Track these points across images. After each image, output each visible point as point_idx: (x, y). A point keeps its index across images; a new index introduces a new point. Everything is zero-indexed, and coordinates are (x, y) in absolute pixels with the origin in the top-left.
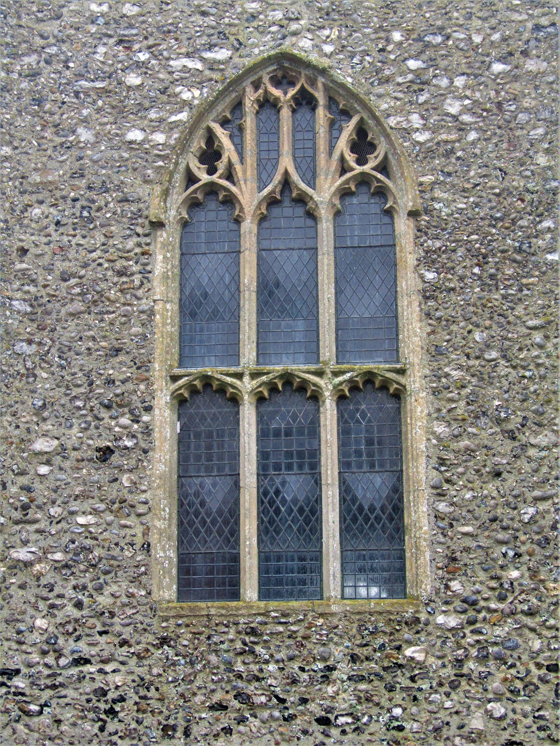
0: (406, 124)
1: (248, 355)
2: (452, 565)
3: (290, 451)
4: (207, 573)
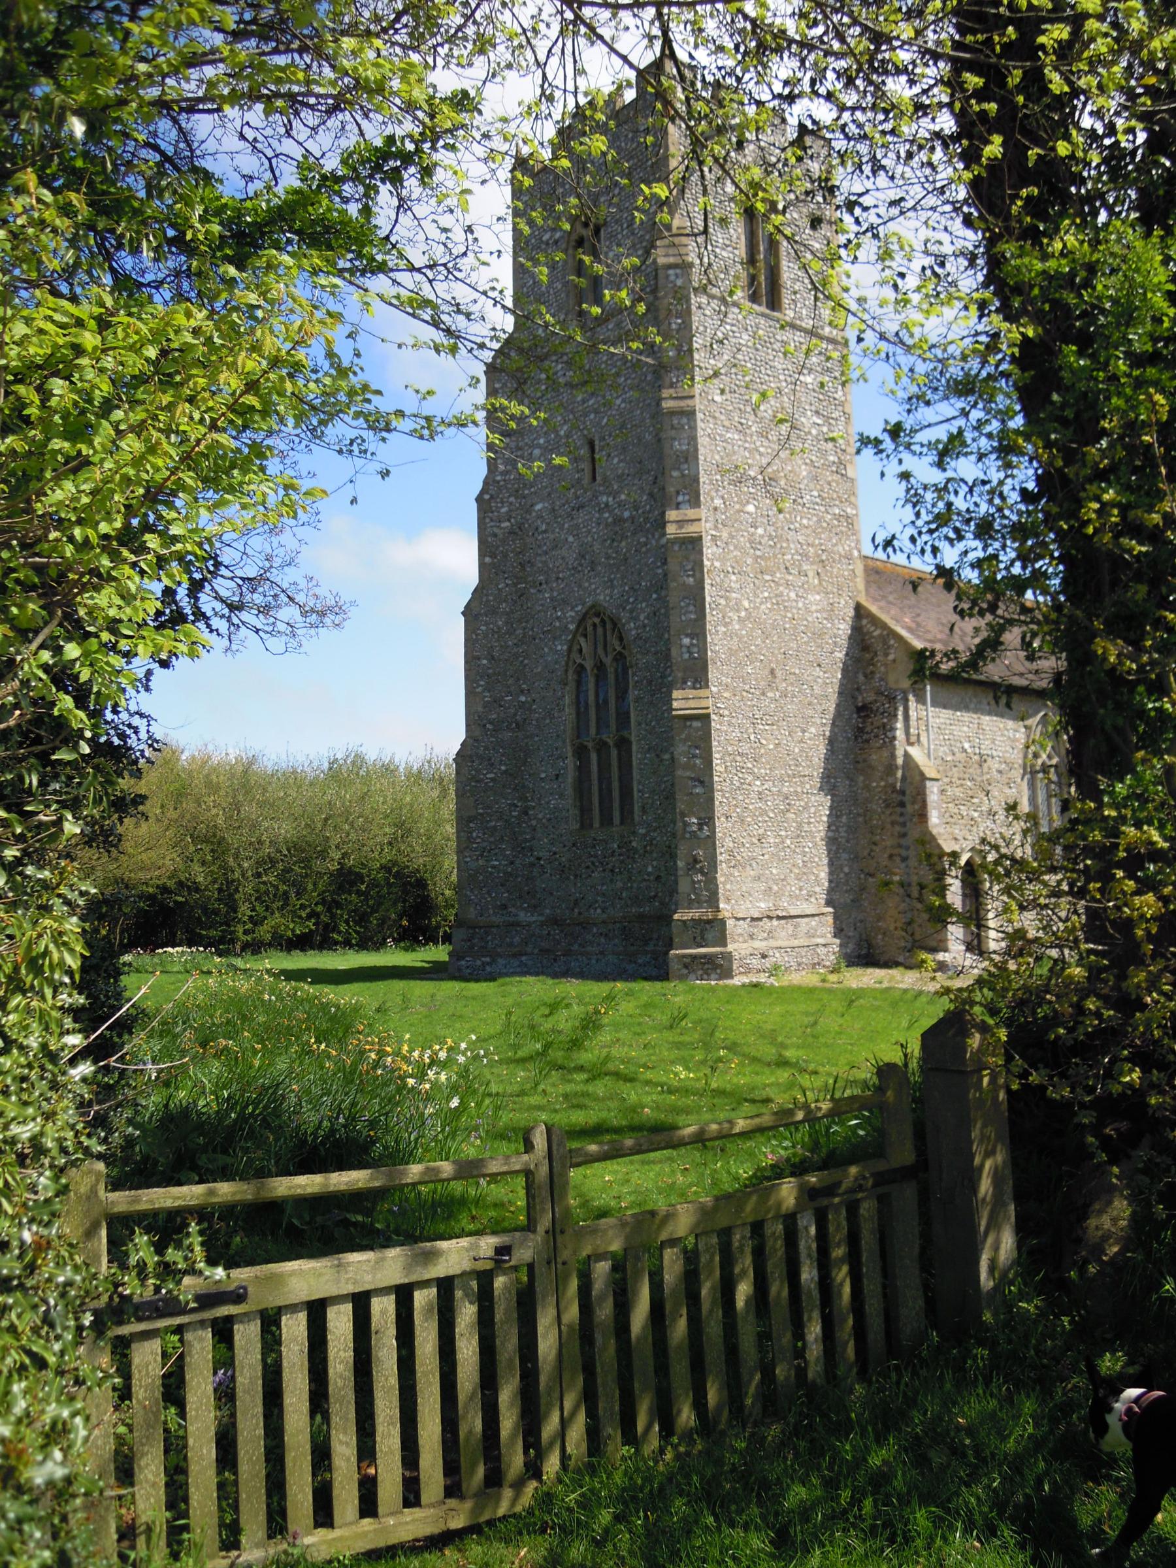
2: (644, 810)
3: (604, 767)
4: (585, 823)
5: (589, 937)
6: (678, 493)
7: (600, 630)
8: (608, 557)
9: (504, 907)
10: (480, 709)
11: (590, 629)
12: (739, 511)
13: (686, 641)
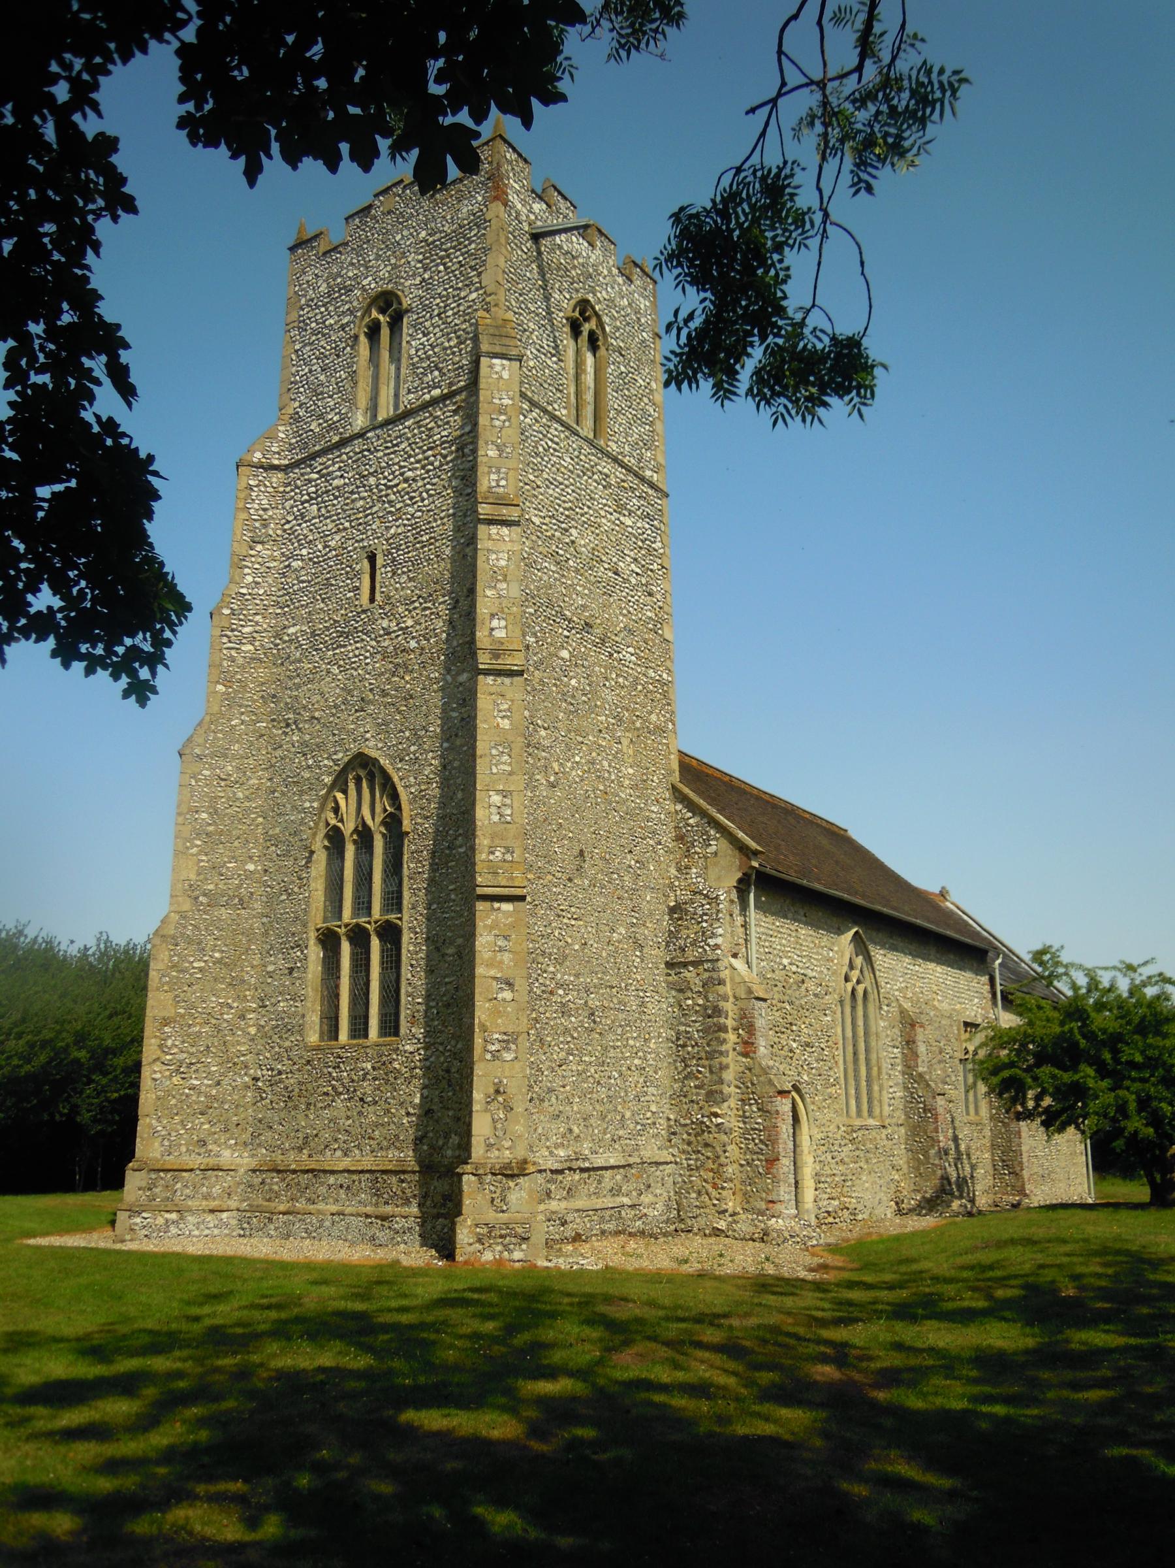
3: (361, 964)
5: (323, 1190)
6: (493, 616)
8: (384, 693)
9: (203, 1143)
10: (193, 876)
11: (352, 786)
13: (496, 799)
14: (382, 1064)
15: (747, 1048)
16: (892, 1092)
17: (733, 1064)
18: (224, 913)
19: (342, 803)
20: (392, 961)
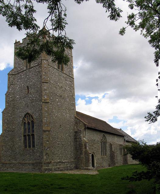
0: (35, 117)
1: (27, 133)
2: (37, 145)
3: (29, 139)
4: (26, 147)
7: (29, 117)
12: (55, 100)
14: (33, 150)
15: (86, 148)
16: (108, 153)
17: (84, 150)
18: (10, 133)
19: (26, 119)
20: (33, 138)
